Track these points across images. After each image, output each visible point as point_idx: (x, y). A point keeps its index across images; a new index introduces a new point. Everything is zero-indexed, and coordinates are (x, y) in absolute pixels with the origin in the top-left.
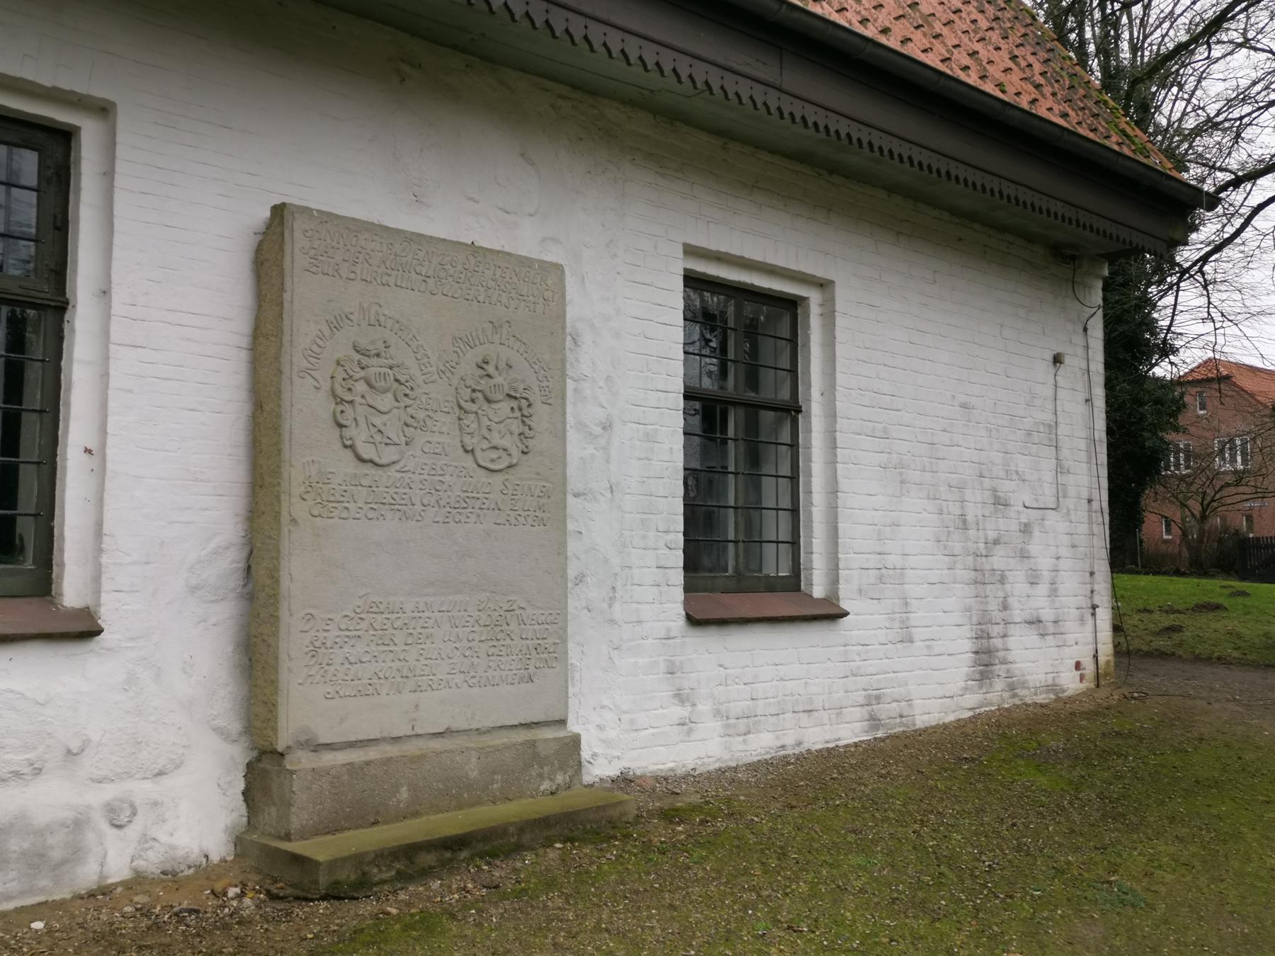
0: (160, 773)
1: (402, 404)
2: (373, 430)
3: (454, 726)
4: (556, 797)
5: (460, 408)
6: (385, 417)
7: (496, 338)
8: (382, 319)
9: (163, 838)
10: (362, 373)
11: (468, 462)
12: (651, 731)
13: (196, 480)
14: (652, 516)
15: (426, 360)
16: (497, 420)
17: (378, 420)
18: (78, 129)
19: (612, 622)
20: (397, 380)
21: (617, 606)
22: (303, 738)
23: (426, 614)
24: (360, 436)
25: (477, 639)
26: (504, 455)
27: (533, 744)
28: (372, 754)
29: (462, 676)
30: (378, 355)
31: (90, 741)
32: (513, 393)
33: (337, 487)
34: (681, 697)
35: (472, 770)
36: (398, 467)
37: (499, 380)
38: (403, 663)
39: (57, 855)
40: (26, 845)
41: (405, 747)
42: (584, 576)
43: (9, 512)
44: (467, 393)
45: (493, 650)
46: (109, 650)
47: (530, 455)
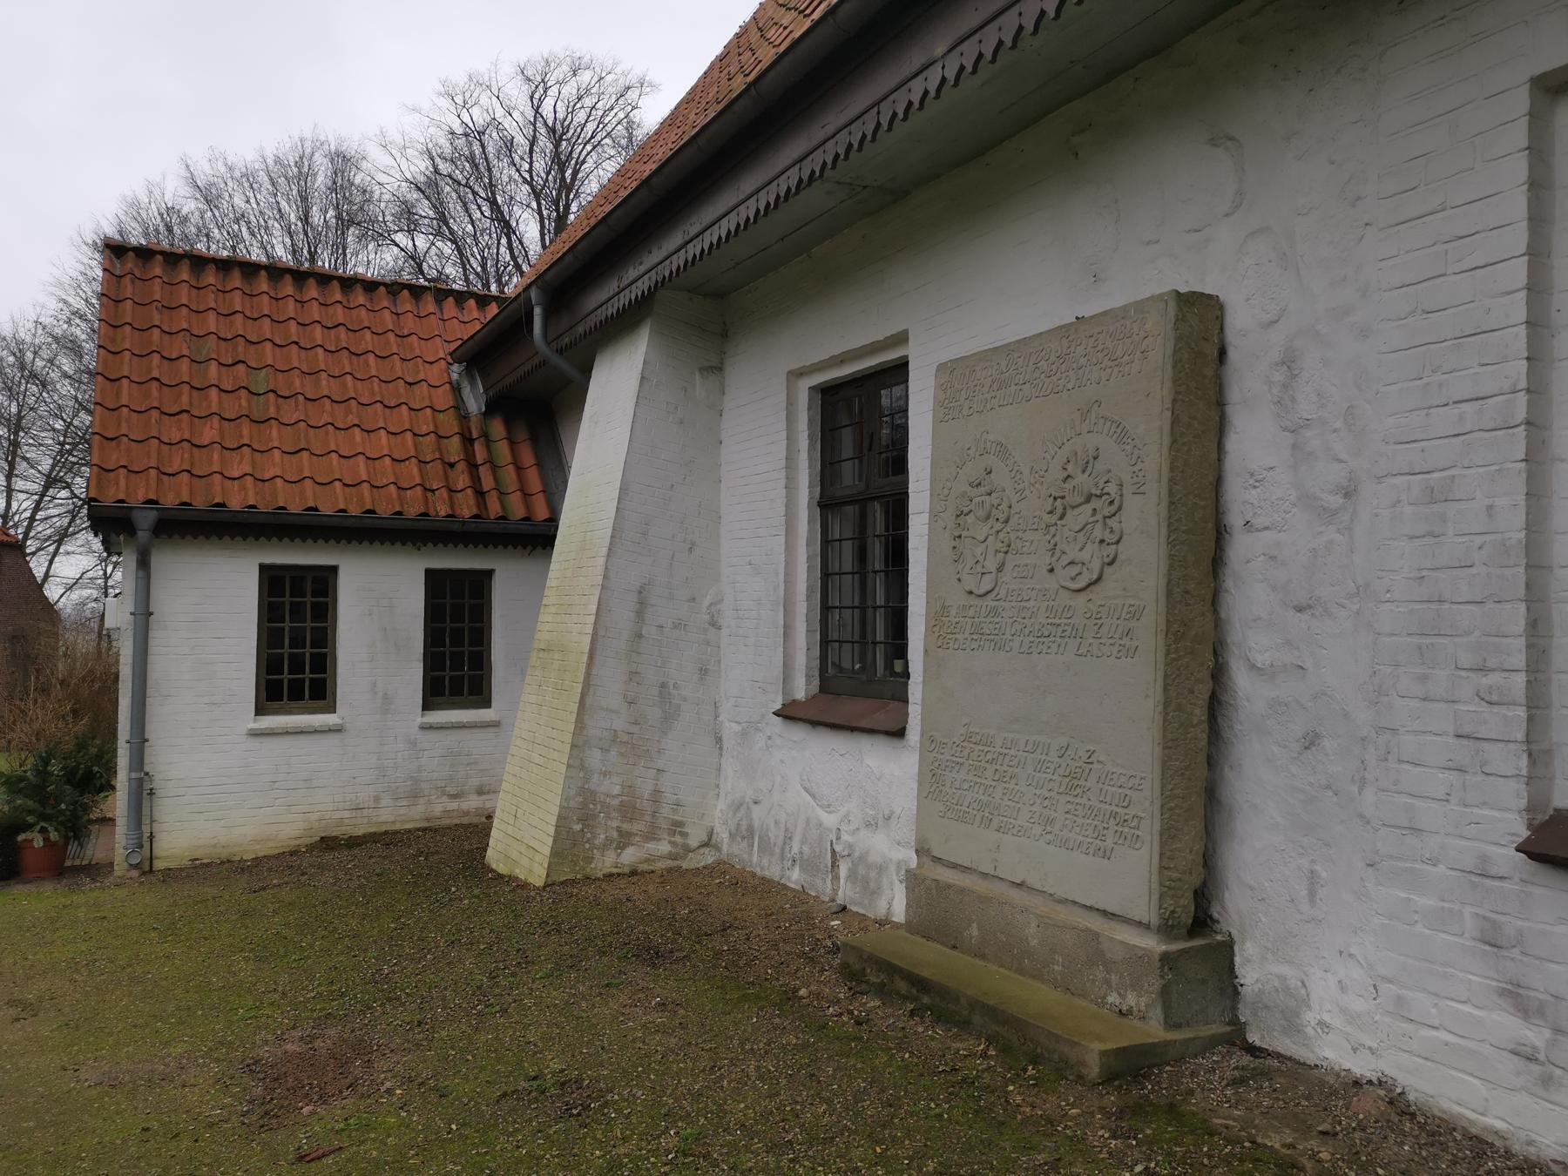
3: (1031, 881)
4: (1124, 1020)
12: (1444, 1035)
23: (1012, 752)
27: (1096, 936)
34: (1516, 997)
42: (1317, 736)
43: (287, 641)
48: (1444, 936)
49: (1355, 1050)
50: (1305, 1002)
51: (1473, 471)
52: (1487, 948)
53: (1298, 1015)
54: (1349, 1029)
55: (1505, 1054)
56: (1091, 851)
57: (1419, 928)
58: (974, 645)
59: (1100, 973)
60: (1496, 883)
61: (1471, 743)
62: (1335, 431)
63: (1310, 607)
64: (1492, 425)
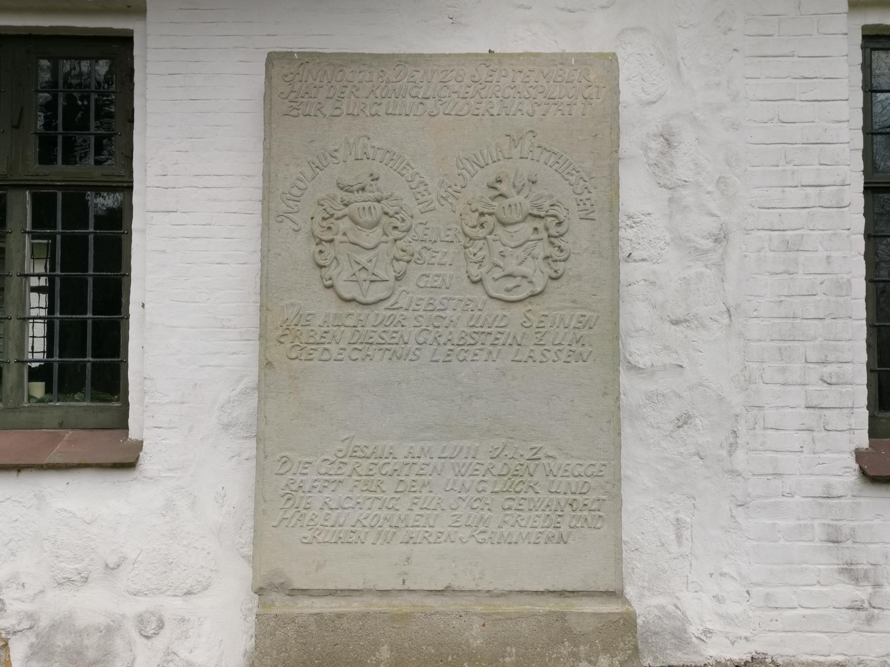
0: (189, 593)
1: (391, 238)
2: (357, 267)
3: (456, 585)
5: (466, 235)
6: (372, 253)
7: (516, 153)
8: (370, 151)
9: (183, 653)
10: (346, 210)
11: (478, 293)
13: (223, 327)
14: (796, 344)
15: (422, 188)
16: (513, 244)
17: (363, 258)
18: (132, 31)
19: (734, 473)
20: (386, 213)
21: (740, 455)
22: (278, 581)
23: (422, 460)
24: (341, 276)
25: (489, 490)
26: (524, 283)
27: (562, 616)
28: (355, 606)
29: (469, 531)
30: (363, 189)
31: (125, 558)
32: (535, 212)
33: (316, 329)
34: (851, 573)
35: (475, 639)
36: (387, 304)
37: (516, 199)
38: (392, 512)
39: (91, 654)
40: (68, 642)
41: (395, 602)
44: (474, 218)
45: (511, 503)
46: (151, 479)
47: (564, 280)
48: (800, 543)
49: (733, 643)
50: (685, 619)
51: (816, 233)
52: (831, 544)
53: (685, 631)
54: (728, 629)
55: (844, 610)
56: (542, 540)
57: (782, 542)
58: (355, 355)
59: (566, 649)
60: (836, 501)
61: (817, 411)
62: (708, 193)
63: (686, 321)
64: (829, 204)
